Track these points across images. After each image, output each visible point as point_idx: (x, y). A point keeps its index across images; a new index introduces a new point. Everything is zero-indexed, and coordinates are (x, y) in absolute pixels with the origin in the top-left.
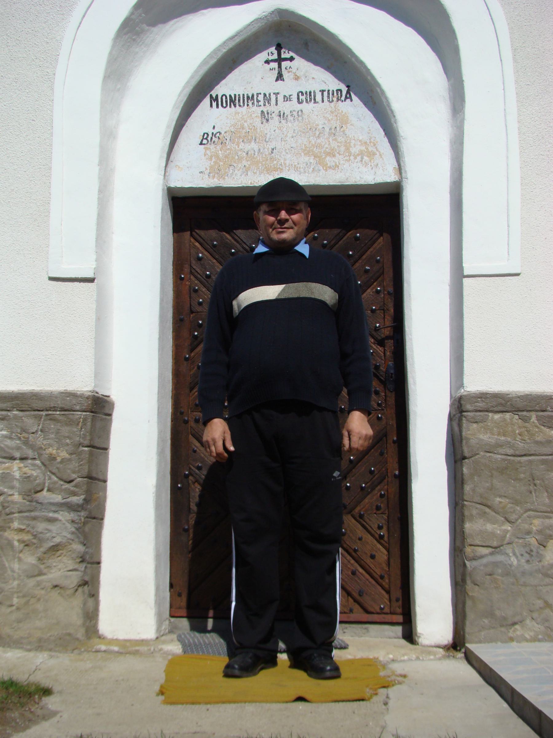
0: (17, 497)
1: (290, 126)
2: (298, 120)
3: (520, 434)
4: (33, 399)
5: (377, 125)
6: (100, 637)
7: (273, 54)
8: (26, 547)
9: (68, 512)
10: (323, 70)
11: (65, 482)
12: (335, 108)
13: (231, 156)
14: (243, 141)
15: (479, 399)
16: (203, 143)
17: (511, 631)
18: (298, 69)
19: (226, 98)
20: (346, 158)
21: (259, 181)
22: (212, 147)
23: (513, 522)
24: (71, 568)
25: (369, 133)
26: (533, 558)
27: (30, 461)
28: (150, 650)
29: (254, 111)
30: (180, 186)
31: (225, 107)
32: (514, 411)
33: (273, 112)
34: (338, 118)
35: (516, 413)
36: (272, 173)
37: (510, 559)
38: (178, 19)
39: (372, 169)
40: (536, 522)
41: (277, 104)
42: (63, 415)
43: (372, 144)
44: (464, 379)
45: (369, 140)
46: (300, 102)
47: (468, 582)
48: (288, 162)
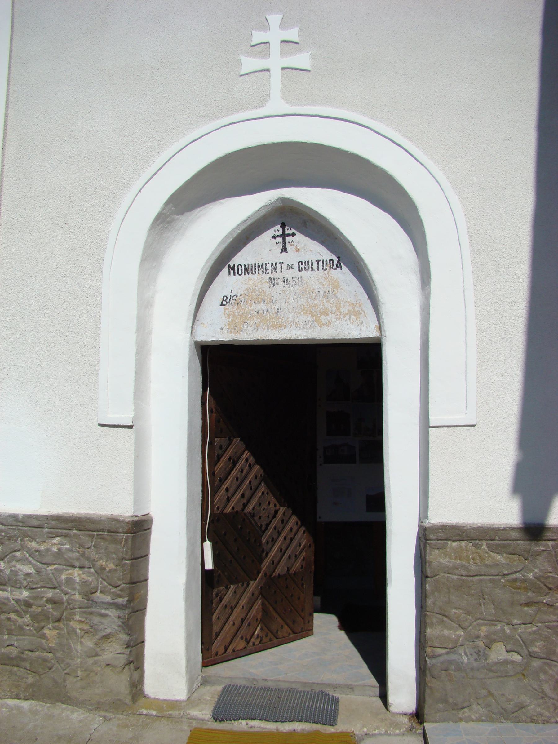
0: (77, 597)
1: (292, 290)
2: (298, 285)
3: (473, 559)
4: (87, 522)
5: (362, 290)
6: (145, 697)
7: (278, 231)
8: (85, 634)
9: (116, 610)
10: (318, 244)
11: (113, 586)
12: (329, 275)
13: (245, 315)
14: (254, 303)
15: (441, 530)
16: (223, 304)
17: (460, 713)
18: (298, 243)
19: (241, 267)
20: (337, 317)
21: (267, 336)
22: (230, 307)
23: (465, 629)
24: (119, 652)
25: (355, 296)
26: (480, 657)
27: (86, 569)
28: (180, 714)
29: (264, 277)
30: (205, 340)
31: (240, 275)
32: (468, 540)
33: (279, 279)
34: (331, 284)
35: (471, 542)
36: (277, 329)
37: (462, 658)
38: (202, 208)
39: (358, 326)
40: (484, 628)
41: (281, 272)
42: (109, 535)
43: (358, 305)
44: (429, 513)
45: (355, 301)
46: (300, 270)
47: (428, 675)
48: (290, 320)
